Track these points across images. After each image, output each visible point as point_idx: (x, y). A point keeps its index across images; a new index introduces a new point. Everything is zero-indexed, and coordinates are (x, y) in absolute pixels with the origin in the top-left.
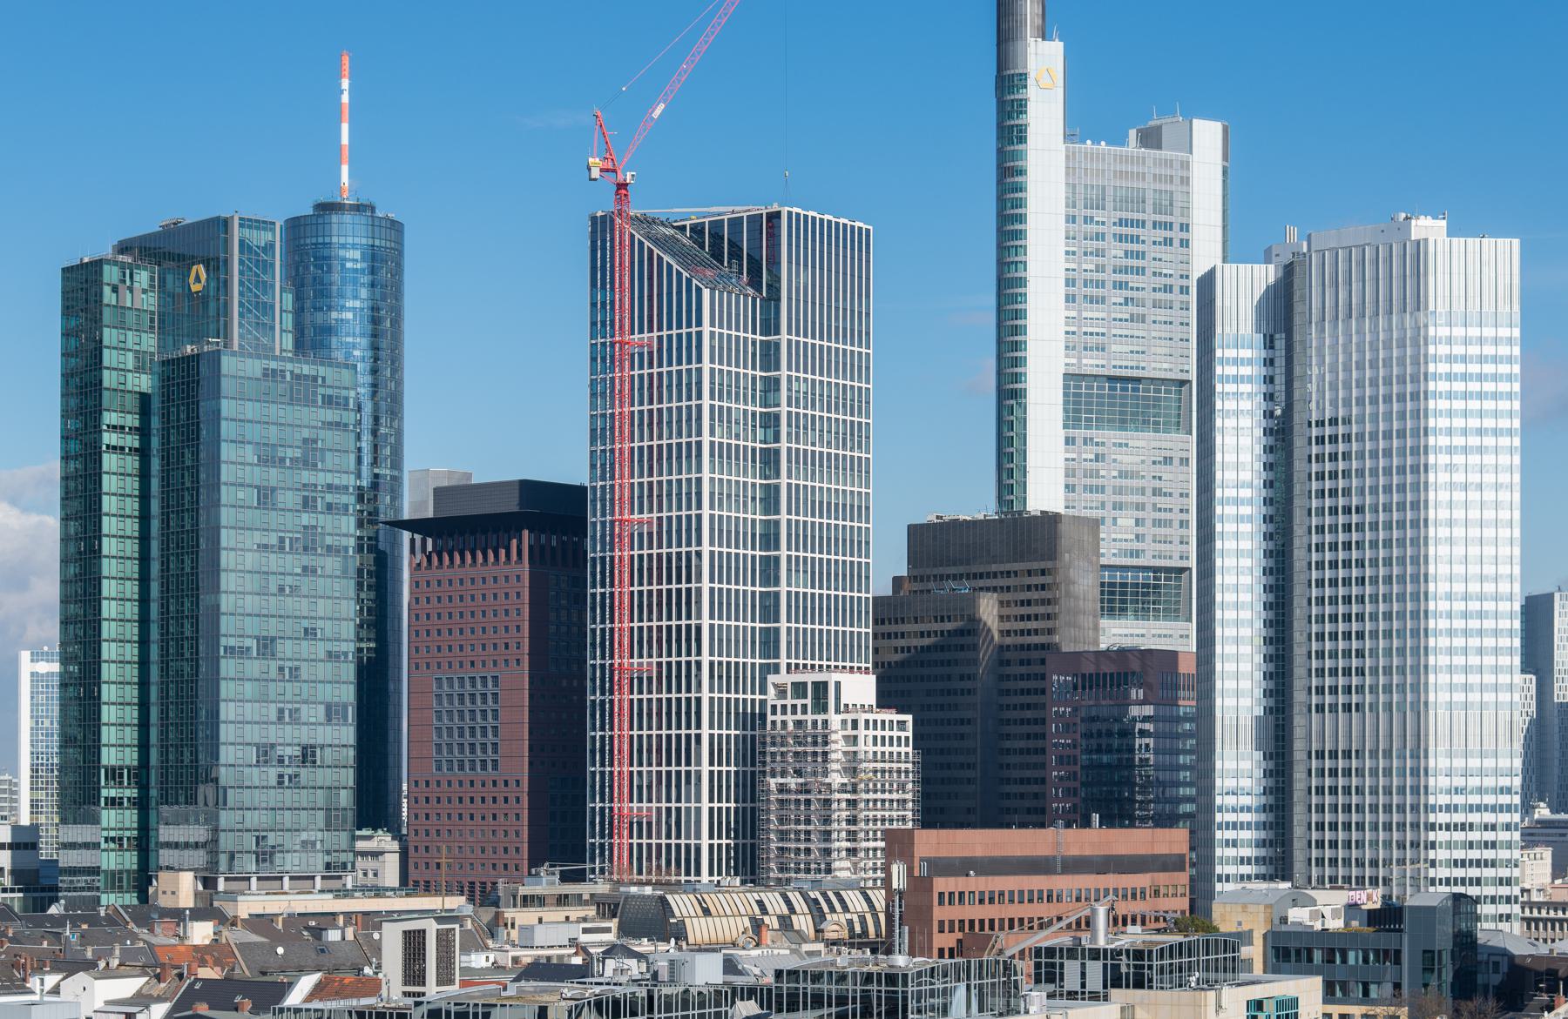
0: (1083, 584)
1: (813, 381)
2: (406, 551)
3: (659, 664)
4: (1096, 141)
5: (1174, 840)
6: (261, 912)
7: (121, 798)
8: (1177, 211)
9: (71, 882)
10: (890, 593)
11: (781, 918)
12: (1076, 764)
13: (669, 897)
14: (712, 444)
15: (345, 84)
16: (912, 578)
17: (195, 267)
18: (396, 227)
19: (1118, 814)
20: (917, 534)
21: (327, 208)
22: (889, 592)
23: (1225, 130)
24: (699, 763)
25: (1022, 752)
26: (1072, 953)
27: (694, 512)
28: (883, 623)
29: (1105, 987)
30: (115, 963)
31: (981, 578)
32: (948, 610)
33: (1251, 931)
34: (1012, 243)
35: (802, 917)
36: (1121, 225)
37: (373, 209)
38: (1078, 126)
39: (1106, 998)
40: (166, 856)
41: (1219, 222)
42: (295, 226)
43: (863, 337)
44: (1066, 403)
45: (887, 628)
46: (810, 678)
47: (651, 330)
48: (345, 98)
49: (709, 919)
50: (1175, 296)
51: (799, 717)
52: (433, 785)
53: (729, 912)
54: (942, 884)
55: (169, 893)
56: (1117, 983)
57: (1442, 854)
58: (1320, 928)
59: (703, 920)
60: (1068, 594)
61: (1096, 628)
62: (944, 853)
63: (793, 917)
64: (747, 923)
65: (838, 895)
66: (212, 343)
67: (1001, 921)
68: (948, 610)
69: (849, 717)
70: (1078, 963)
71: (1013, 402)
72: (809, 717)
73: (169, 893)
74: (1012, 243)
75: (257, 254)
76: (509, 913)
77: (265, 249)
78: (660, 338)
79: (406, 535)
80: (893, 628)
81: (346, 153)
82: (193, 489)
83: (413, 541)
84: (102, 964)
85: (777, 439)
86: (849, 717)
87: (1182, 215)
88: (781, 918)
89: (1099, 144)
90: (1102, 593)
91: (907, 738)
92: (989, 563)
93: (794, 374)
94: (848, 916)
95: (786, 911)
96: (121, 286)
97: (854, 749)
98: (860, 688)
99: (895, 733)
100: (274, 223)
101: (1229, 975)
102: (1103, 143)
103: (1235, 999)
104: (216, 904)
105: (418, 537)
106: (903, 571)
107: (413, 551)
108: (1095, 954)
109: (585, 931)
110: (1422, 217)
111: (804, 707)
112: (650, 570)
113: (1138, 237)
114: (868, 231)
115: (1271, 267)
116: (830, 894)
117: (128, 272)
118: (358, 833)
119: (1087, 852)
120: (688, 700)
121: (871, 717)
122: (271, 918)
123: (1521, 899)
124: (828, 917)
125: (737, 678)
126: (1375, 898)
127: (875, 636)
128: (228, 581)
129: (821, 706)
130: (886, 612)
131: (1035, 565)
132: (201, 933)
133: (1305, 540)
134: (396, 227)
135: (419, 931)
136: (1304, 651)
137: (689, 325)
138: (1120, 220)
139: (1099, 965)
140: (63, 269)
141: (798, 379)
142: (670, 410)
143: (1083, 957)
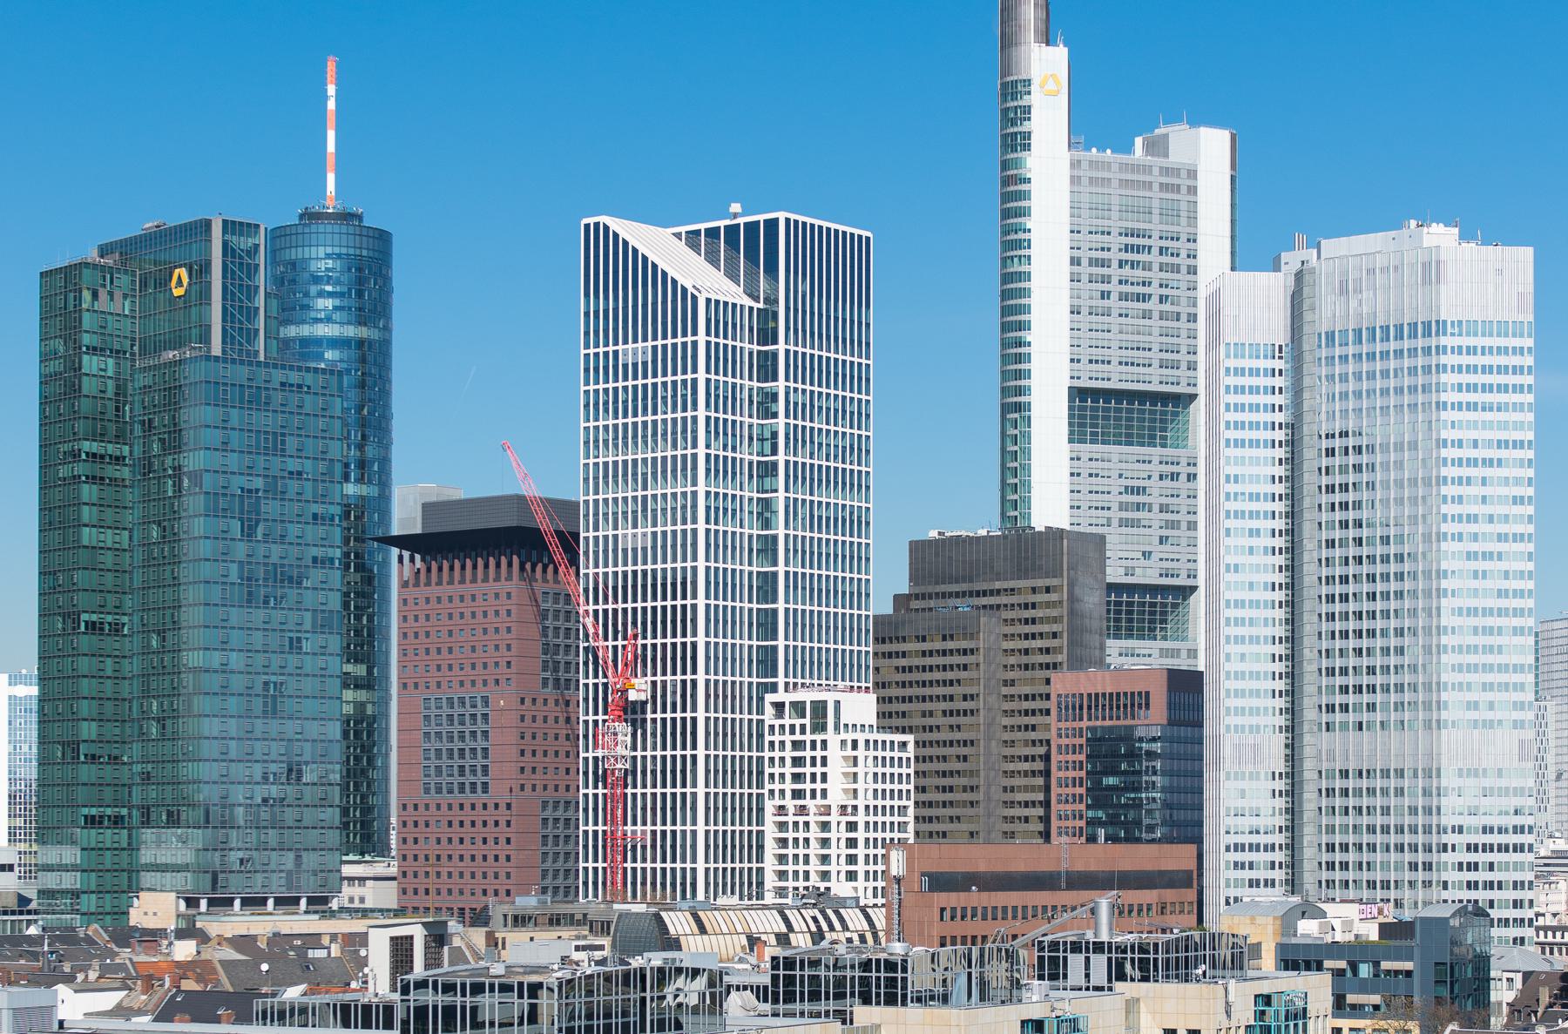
1: (812, 392)
2: (397, 568)
3: (654, 833)
4: (1102, 149)
6: (244, 932)
7: (102, 623)
9: (49, 905)
10: (891, 611)
11: (778, 936)
12: (1081, 769)
13: (663, 914)
14: (708, 456)
15: (331, 90)
17: (177, 271)
18: (383, 238)
20: (921, 553)
22: (888, 609)
25: (1026, 774)
26: (1076, 947)
27: (689, 677)
28: (884, 641)
29: (1110, 980)
30: (93, 975)
31: (984, 595)
32: (951, 628)
33: (1259, 944)
34: (1015, 253)
35: (800, 936)
36: (1126, 251)
39: (1110, 989)
41: (1227, 172)
42: (279, 235)
43: (864, 347)
44: (1071, 416)
45: (887, 647)
47: (645, 339)
48: (331, 105)
49: (704, 937)
51: (798, 737)
52: (421, 808)
53: (725, 930)
55: (151, 914)
56: (1121, 977)
57: (1448, 378)
58: (1330, 941)
59: (698, 938)
61: (1102, 648)
62: (945, 868)
63: (791, 935)
64: (744, 941)
65: (837, 913)
66: (195, 348)
67: (1005, 909)
68: (951, 628)
69: (850, 737)
70: (1081, 957)
71: (1016, 415)
72: (808, 737)
73: (151, 914)
74: (1015, 253)
75: (241, 257)
77: (248, 252)
78: (655, 348)
79: (395, 551)
80: (894, 647)
81: (331, 161)
82: (175, 476)
84: (80, 977)
85: (774, 452)
86: (850, 737)
87: (1189, 226)
88: (778, 936)
89: (1104, 151)
90: (1108, 611)
91: (908, 759)
92: (992, 580)
93: (792, 385)
94: (848, 935)
95: (784, 929)
96: (101, 290)
97: (854, 770)
98: (861, 707)
99: (896, 754)
100: (257, 226)
101: (1237, 973)
102: (1109, 151)
103: (1242, 995)
104: (198, 925)
105: (406, 554)
106: (904, 589)
108: (1099, 947)
109: (577, 948)
110: (1434, 225)
111: (803, 727)
112: (644, 586)
113: (1144, 488)
114: (868, 239)
116: (830, 912)
117: (108, 276)
118: (344, 858)
119: (1092, 868)
120: (684, 645)
121: (872, 737)
122: (254, 938)
123: (1535, 923)
124: (827, 935)
125: (734, 623)
126: (1386, 912)
127: (876, 654)
129: (820, 727)
130: (886, 631)
131: (1040, 583)
132: (184, 950)
133: (1315, 556)
134: (383, 238)
135: (406, 937)
136: (1315, 667)
137: (685, 334)
138: (1126, 245)
139: (1103, 958)
140: (42, 274)
142: (665, 421)
143: (1087, 951)
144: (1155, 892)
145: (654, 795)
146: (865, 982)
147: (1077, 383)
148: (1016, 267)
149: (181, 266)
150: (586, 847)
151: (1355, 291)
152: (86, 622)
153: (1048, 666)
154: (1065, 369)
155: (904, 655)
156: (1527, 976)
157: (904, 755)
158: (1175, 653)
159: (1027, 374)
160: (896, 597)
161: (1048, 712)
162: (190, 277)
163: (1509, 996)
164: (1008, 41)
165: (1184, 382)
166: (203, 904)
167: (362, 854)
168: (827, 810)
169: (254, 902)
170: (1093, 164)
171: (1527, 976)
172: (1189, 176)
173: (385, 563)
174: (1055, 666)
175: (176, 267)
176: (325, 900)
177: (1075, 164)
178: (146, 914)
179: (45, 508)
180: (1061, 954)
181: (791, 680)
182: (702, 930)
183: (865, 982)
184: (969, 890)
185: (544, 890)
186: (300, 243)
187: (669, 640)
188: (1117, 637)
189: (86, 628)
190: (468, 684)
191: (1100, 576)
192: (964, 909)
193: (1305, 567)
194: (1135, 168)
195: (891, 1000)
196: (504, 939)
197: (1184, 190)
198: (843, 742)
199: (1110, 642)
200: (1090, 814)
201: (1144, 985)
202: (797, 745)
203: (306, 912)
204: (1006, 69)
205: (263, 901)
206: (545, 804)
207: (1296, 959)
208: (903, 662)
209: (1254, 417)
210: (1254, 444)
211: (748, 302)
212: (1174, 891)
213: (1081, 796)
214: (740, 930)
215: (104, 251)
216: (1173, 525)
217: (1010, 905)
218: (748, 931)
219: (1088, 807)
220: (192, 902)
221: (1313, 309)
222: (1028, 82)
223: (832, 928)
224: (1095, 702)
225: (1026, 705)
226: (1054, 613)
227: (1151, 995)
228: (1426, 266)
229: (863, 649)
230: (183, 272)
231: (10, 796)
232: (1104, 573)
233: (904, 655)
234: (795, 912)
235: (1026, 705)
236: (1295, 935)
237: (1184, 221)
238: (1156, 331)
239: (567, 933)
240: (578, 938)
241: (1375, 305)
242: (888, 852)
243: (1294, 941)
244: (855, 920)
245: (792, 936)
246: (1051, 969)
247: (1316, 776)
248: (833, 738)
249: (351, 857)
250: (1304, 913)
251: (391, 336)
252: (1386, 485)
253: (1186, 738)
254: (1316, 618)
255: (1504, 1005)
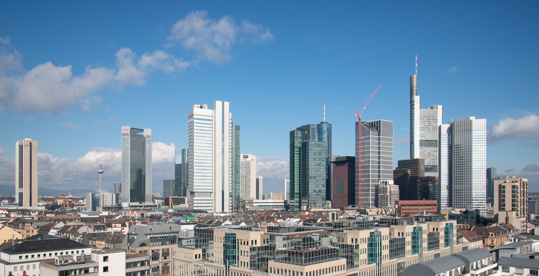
0: (422, 168)
5: (435, 202)
16: (398, 168)
19: (427, 198)
22: (395, 169)
23: (443, 106)
24: (370, 192)
37: (328, 123)
38: (421, 107)
40: (303, 204)
42: (318, 125)
44: (420, 144)
46: (385, 181)
50: (435, 129)
51: (383, 186)
54: (402, 208)
56: (427, 221)
60: (420, 169)
61: (424, 174)
64: (376, 212)
69: (390, 186)
72: (385, 186)
76: (345, 211)
79: (332, 163)
83: (333, 164)
84: (295, 217)
85: (380, 150)
86: (390, 186)
98: (391, 182)
107: (333, 165)
108: (424, 217)
109: (355, 213)
111: (384, 185)
115: (449, 124)
121: (393, 186)
128: (310, 170)
129: (386, 184)
130: (395, 172)
132: (307, 213)
134: (331, 125)
136: (454, 176)
145: (365, 189)
146: (392, 222)
157: (397, 188)
170: (423, 111)
181: (382, 179)
182: (371, 211)
183: (392, 222)
187: (365, 183)
194: (429, 111)
195: (396, 224)
198: (389, 187)
207: (452, 217)
221: (454, 129)
222: (414, 101)
223: (388, 211)
237: (435, 118)
244: (391, 210)
246: (417, 219)
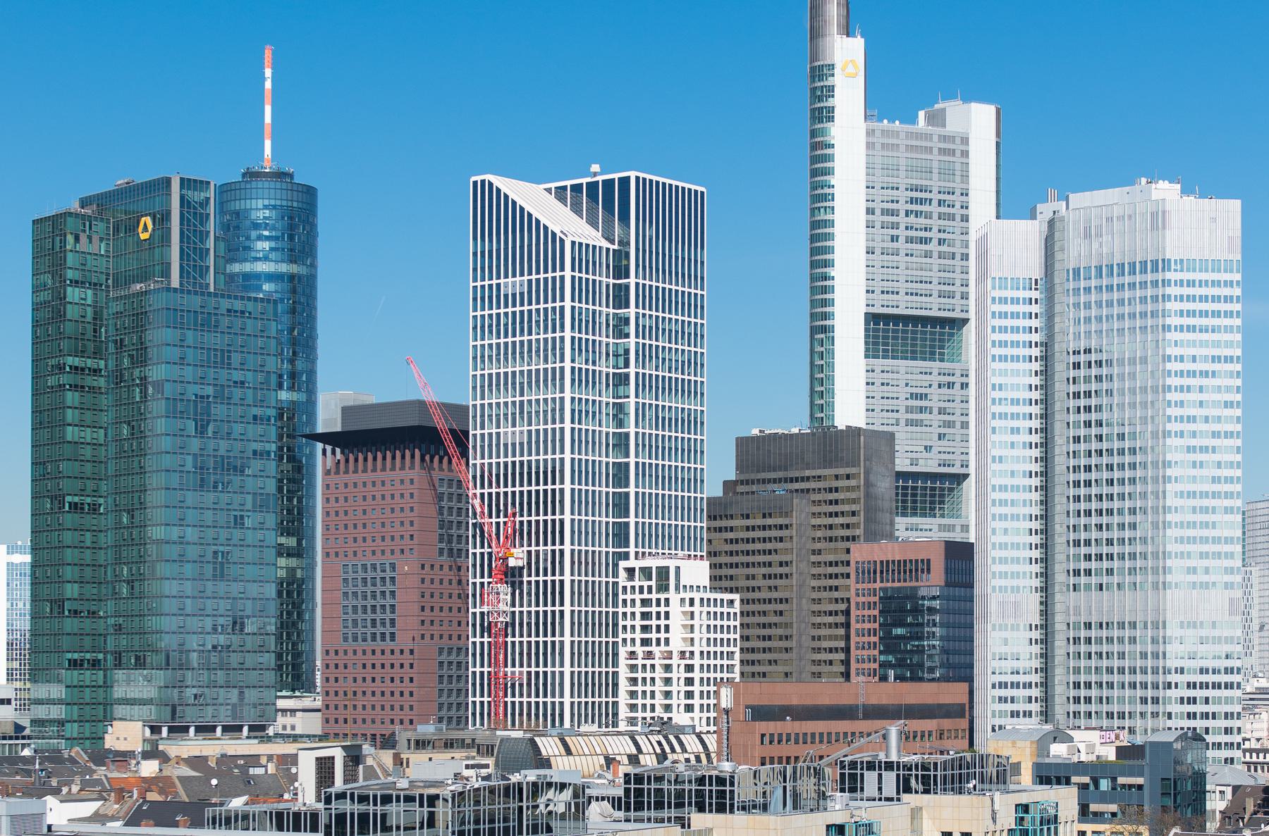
1: (657, 317)
2: (322, 459)
3: (529, 673)
4: (892, 120)
6: (198, 754)
7: (82, 504)
8: (958, 179)
9: (40, 731)
10: (721, 494)
11: (630, 757)
12: (875, 622)
13: (537, 739)
14: (573, 369)
15: (268, 72)
17: (143, 219)
18: (310, 192)
20: (746, 447)
21: (251, 175)
22: (718, 492)
25: (830, 626)
26: (871, 766)
27: (557, 547)
28: (715, 519)
29: (898, 793)
30: (75, 789)
31: (797, 481)
32: (770, 508)
33: (1019, 763)
34: (822, 204)
35: (647, 757)
36: (912, 203)
39: (899, 800)
41: (993, 139)
42: (226, 190)
43: (699, 280)
44: (867, 337)
45: (718, 523)
47: (522, 274)
48: (268, 85)
49: (570, 757)
51: (646, 596)
52: (341, 653)
53: (587, 752)
55: (122, 739)
56: (908, 790)
57: (1172, 306)
58: (1076, 760)
59: (565, 758)
61: (892, 524)
62: (765, 702)
63: (640, 756)
64: (602, 761)
65: (677, 738)
66: (158, 281)
67: (813, 735)
68: (770, 508)
69: (688, 595)
70: (875, 774)
71: (823, 336)
72: (654, 596)
73: (122, 739)
74: (822, 204)
75: (195, 208)
77: (201, 204)
78: (530, 281)
79: (320, 446)
80: (724, 523)
81: (268, 130)
82: (141, 384)
84: (65, 790)
85: (627, 365)
86: (688, 595)
87: (962, 182)
88: (630, 757)
89: (894, 122)
90: (897, 494)
91: (735, 614)
92: (803, 469)
93: (641, 311)
94: (686, 756)
95: (634, 751)
96: (82, 235)
97: (691, 622)
98: (697, 572)
99: (725, 610)
100: (208, 183)
101: (1001, 786)
102: (897, 122)
104: (161, 748)
105: (329, 448)
106: (732, 476)
108: (889, 766)
109: (467, 767)
110: (1161, 182)
111: (650, 588)
112: (521, 474)
113: (926, 395)
114: (702, 193)
116: (671, 737)
117: (88, 223)
118: (279, 694)
119: (884, 702)
120: (554, 521)
121: (706, 596)
122: (205, 758)
123: (1242, 747)
124: (670, 756)
125: (594, 503)
126: (1121, 737)
127: (709, 529)
129: (663, 588)
130: (717, 510)
131: (842, 471)
132: (149, 768)
134: (310, 192)
135: (329, 758)
136: (1064, 539)
137: (554, 270)
138: (912, 198)
139: (893, 775)
140: (34, 221)
141: (644, 315)
142: (538, 341)
143: (880, 769)
144: (935, 721)
145: (529, 643)
146: (700, 794)
147: (871, 310)
148: (822, 216)
149: (146, 215)
150: (474, 685)
151: (1096, 235)
152: (70, 503)
153: (848, 539)
154: (862, 298)
155: (732, 529)
156: (1236, 789)
157: (732, 611)
158: (951, 528)
159: (831, 303)
160: (725, 483)
161: (848, 576)
162: (154, 224)
163: (1221, 805)
164: (816, 33)
165: (958, 309)
166: (165, 731)
167: (293, 690)
168: (669, 655)
169: (206, 730)
170: (885, 133)
171: (1236, 789)
172: (962, 142)
173: (312, 455)
174: (854, 538)
175: (142, 216)
176: (263, 728)
177: (870, 133)
178: (118, 739)
179: (36, 411)
180: (859, 772)
181: (640, 550)
182: (569, 752)
183: (700, 794)
184: (784, 719)
185: (440, 720)
186: (243, 197)
187: (541, 518)
188: (904, 515)
189: (70, 508)
190: (379, 553)
191: (890, 466)
192: (780, 735)
193: (1057, 458)
194: (919, 136)
195: (721, 809)
196: (408, 759)
197: (958, 153)
198: (682, 600)
199: (898, 519)
200: (882, 658)
201: (926, 796)
202: (645, 602)
203: (248, 738)
204: (814, 56)
205: (213, 729)
206: (441, 650)
208: (731, 535)
209: (1015, 337)
210: (1015, 359)
211: (605, 244)
212: (950, 720)
213: (875, 643)
214: (599, 752)
215: (84, 203)
216: (950, 424)
217: (817, 731)
218: (605, 753)
219: (881, 653)
220: (155, 730)
221: (1062, 250)
222: (832, 67)
223: (673, 750)
224: (886, 568)
225: (830, 570)
226: (853, 495)
227: (932, 804)
228: (1154, 215)
229: (699, 524)
230: (148, 220)
231: (8, 644)
232: (894, 463)
233: (732, 529)
234: (644, 737)
235: (830, 570)
236: (1048, 756)
238: (935, 268)
239: (459, 754)
240: (468, 758)
241: (1113, 247)
242: (719, 689)
243: (1047, 761)
245: (641, 757)
246: (851, 783)
247: (1065, 627)
248: (674, 597)
249: (284, 693)
250: (1055, 738)
251: (316, 272)
252: (1122, 392)
253: (960, 596)
254: (1065, 500)
255: (1218, 813)
